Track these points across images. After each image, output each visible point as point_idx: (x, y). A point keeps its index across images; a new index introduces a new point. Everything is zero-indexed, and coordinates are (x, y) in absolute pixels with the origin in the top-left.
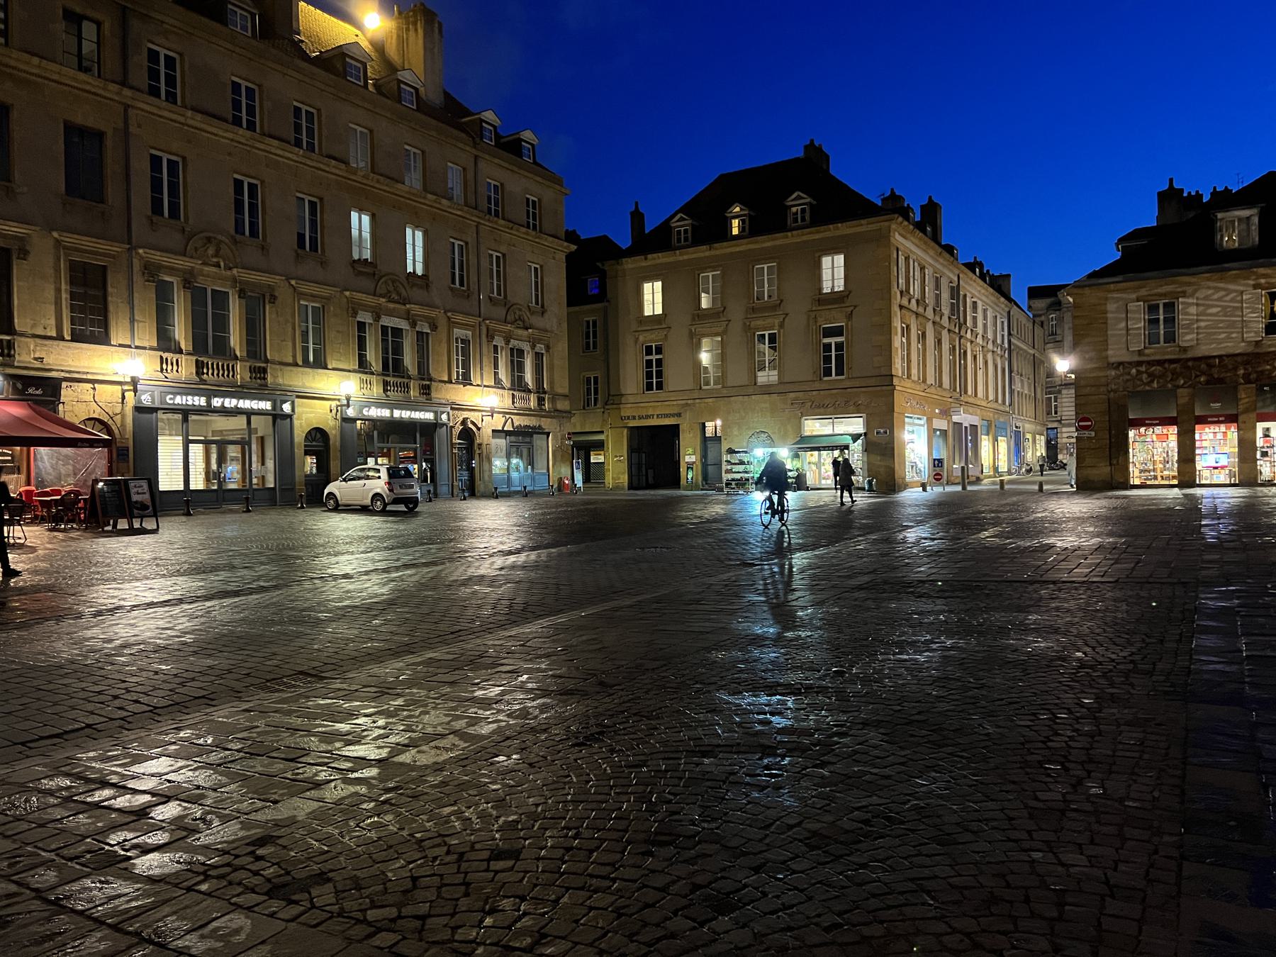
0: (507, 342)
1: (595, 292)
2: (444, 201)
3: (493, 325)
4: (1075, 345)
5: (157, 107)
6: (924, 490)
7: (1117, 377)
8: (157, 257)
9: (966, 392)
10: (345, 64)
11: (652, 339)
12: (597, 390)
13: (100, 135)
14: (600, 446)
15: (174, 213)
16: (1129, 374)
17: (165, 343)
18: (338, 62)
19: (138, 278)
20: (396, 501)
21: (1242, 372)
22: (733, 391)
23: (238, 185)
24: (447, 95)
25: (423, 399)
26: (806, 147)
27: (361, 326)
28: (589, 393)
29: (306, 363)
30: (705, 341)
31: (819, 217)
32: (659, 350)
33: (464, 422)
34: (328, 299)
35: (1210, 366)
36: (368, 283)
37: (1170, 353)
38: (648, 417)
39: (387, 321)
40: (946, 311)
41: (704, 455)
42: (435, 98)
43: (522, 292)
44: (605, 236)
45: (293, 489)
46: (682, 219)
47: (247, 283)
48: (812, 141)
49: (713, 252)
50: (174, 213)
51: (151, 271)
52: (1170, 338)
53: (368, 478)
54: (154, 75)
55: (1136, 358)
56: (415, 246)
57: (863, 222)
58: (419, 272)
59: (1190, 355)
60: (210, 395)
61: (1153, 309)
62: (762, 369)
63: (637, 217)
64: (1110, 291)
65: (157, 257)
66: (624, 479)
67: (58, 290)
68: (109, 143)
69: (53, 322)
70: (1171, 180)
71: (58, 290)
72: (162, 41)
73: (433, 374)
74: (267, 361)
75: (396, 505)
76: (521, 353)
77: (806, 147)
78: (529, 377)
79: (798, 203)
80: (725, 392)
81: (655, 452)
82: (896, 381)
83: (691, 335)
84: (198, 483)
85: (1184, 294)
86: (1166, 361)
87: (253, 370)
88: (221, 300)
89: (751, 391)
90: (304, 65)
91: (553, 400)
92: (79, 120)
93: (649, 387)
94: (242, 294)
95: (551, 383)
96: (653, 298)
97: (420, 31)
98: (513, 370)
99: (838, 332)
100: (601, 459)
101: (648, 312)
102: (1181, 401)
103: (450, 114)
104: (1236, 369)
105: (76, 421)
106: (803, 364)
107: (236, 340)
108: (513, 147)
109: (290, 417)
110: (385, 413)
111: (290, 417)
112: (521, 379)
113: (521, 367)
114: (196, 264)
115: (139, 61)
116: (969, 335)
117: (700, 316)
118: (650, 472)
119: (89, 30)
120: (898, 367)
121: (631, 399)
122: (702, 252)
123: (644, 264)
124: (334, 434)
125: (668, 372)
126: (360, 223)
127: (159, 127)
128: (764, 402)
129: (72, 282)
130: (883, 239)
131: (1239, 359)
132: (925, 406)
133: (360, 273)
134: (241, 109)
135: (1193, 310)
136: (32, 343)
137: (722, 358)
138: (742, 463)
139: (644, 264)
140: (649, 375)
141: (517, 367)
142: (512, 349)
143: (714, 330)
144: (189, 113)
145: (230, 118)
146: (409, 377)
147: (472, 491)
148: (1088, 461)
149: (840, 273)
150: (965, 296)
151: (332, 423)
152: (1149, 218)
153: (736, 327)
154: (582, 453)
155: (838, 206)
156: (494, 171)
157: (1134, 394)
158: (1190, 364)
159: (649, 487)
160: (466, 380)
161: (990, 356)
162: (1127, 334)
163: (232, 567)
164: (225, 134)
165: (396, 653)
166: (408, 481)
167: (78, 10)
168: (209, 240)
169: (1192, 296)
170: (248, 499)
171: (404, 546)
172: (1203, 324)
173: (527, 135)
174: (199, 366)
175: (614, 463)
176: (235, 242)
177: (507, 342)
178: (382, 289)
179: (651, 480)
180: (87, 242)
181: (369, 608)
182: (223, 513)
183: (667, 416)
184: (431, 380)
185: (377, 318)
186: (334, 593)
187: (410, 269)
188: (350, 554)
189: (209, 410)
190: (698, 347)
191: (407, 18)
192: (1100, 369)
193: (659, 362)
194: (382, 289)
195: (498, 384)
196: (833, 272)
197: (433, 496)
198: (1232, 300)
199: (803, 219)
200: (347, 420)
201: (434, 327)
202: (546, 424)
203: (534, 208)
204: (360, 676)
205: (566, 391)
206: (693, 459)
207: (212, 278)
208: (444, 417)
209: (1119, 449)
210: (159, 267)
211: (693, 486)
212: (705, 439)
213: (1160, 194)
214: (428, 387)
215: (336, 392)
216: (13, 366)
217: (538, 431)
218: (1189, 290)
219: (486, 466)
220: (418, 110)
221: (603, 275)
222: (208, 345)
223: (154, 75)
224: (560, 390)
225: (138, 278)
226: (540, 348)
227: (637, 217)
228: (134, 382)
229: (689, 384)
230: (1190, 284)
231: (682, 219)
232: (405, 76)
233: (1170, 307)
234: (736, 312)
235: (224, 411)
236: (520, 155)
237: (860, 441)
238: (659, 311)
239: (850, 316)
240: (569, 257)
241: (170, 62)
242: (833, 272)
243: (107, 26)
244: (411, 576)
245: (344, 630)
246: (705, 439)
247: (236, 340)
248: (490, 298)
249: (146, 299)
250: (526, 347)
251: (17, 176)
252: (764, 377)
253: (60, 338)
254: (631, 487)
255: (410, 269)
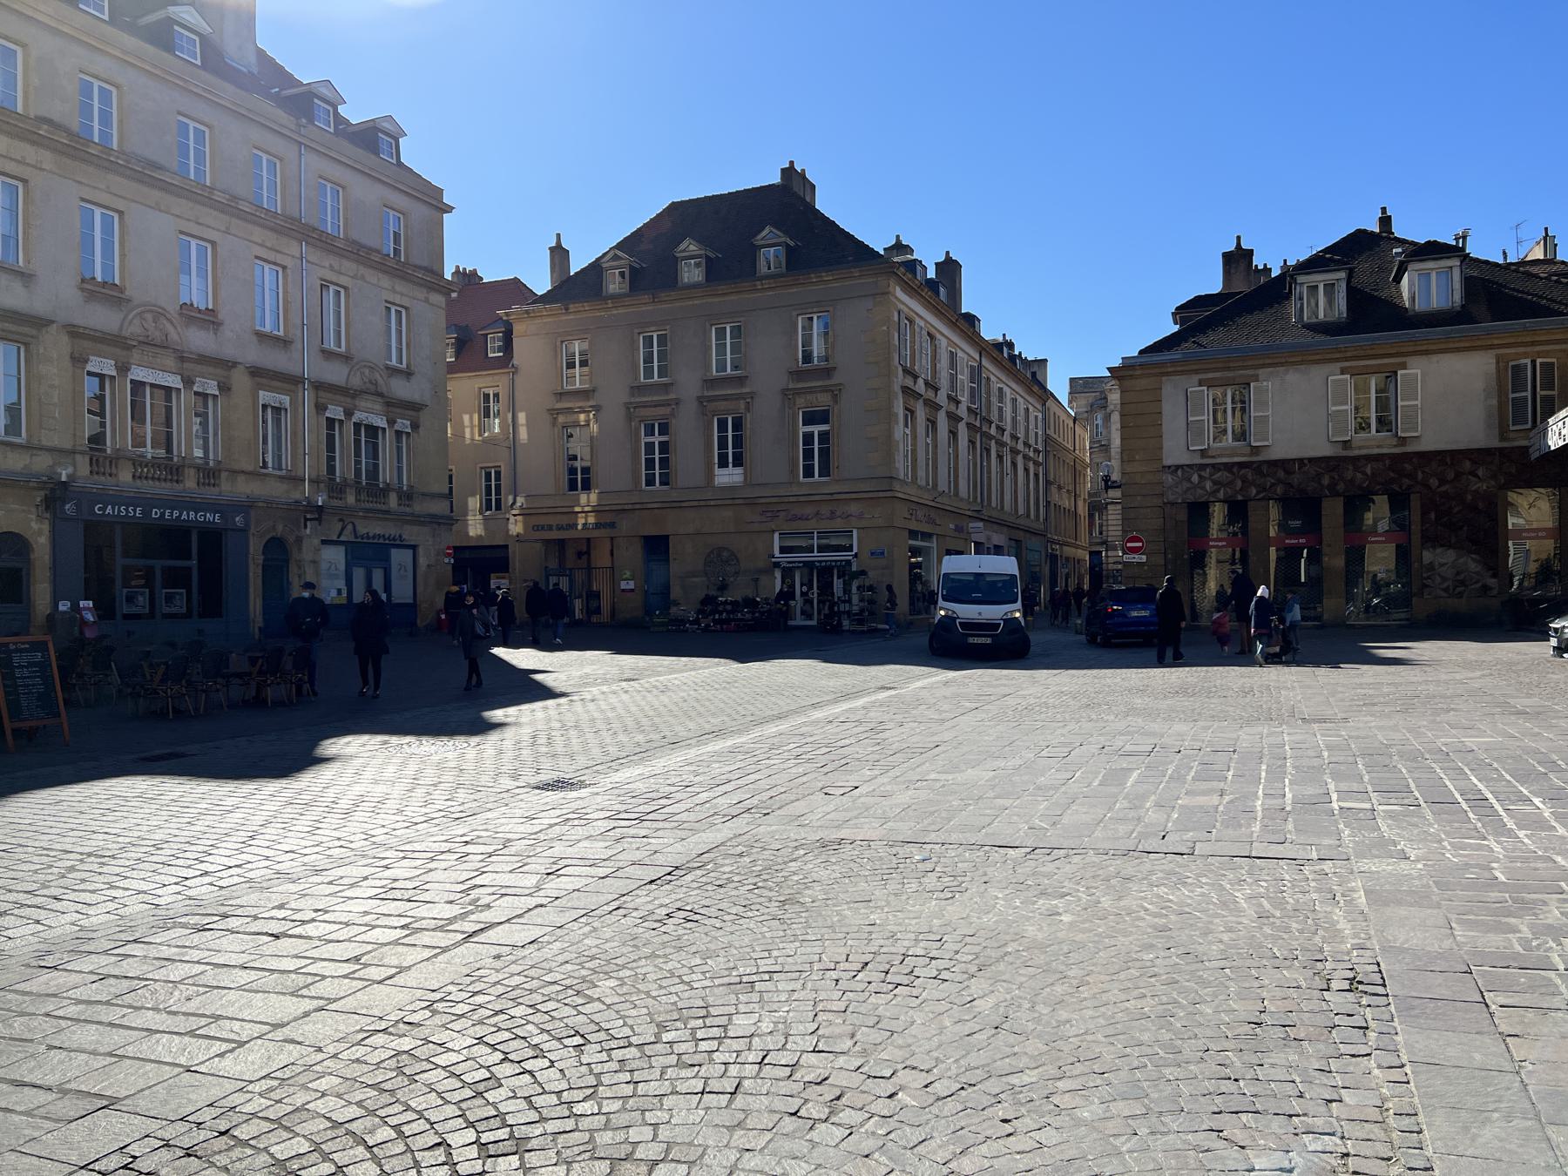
16: (1189, 480)
32: (664, 430)
48: (792, 163)
52: (1242, 435)
55: (1198, 460)
59: (1409, 449)
63: (559, 254)
70: (1239, 238)
79: (770, 255)
140: (664, 462)
142: (357, 426)
152: (1212, 282)
161: (1020, 459)
213: (1225, 255)
220: (204, 67)
227: (559, 254)
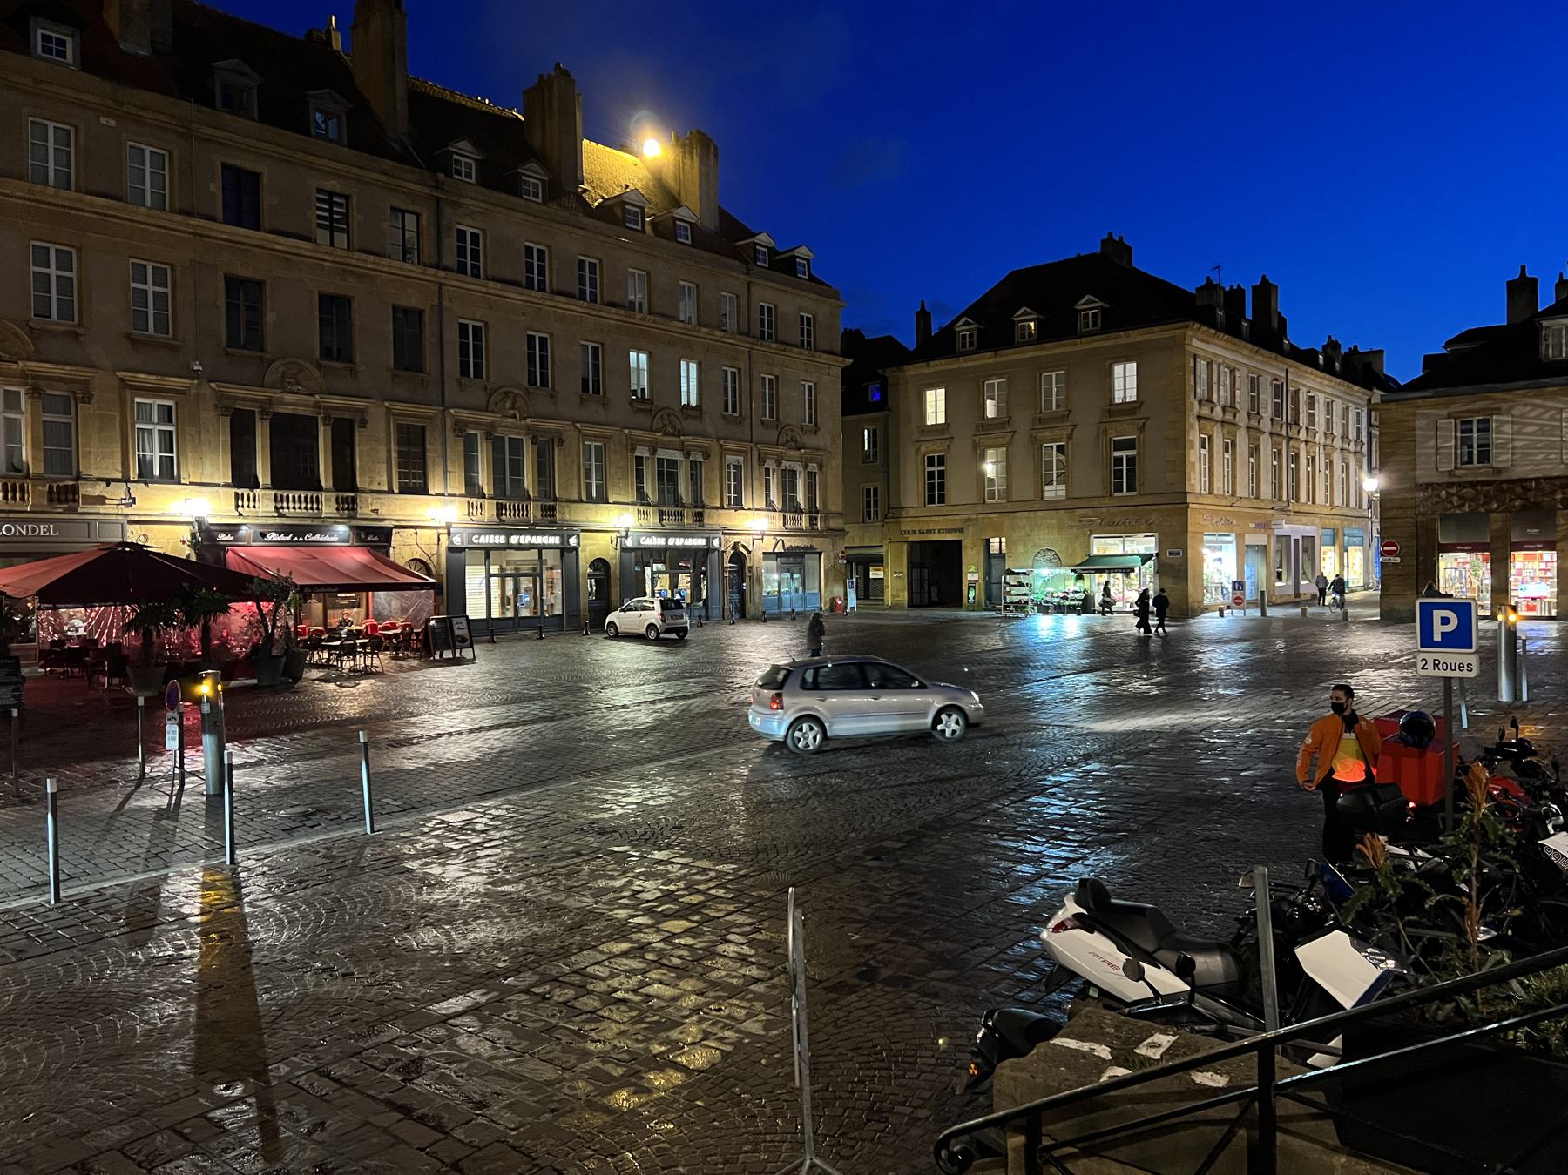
0: (779, 464)
1: (877, 398)
2: (718, 333)
3: (765, 449)
4: (1382, 466)
5: (467, 283)
6: (1221, 615)
7: (1426, 499)
8: (465, 414)
9: (1298, 500)
10: (624, 211)
11: (935, 450)
12: (874, 500)
13: (421, 313)
14: (879, 561)
15: (478, 374)
17: (472, 489)
18: (617, 211)
19: (450, 434)
20: (668, 631)
21: (1559, 496)
22: (1019, 505)
23: (531, 339)
24: (722, 212)
25: (696, 526)
26: (1103, 242)
27: (639, 460)
28: (869, 506)
29: (590, 500)
30: (990, 452)
31: (1111, 322)
32: (941, 461)
33: (735, 546)
34: (609, 438)
35: (1526, 490)
36: (643, 420)
37: (1486, 474)
38: (929, 532)
39: (663, 454)
40: (1267, 414)
41: (988, 572)
42: (711, 223)
43: (795, 411)
44: (890, 337)
45: (578, 616)
46: (966, 323)
47: (537, 430)
48: (1110, 235)
49: (998, 359)
50: (478, 374)
51: (460, 427)
52: (1485, 456)
53: (644, 609)
54: (461, 252)
55: (1446, 479)
56: (689, 375)
57: (1156, 329)
58: (693, 404)
59: (1504, 477)
60: (508, 533)
61: (1466, 427)
62: (1050, 483)
63: (923, 317)
64: (1419, 407)
65: (465, 414)
66: (904, 596)
67: (389, 451)
68: (427, 318)
69: (385, 478)
70: (1523, 268)
71: (389, 451)
72: (471, 222)
73: (706, 502)
74: (555, 500)
75: (669, 636)
76: (793, 473)
77: (1103, 242)
78: (801, 497)
79: (1089, 305)
80: (1010, 507)
81: (936, 570)
82: (1190, 499)
83: (975, 446)
84: (496, 614)
85: (1499, 411)
86: (1478, 483)
87: (543, 508)
88: (516, 445)
89: (1037, 506)
90: (584, 220)
91: (825, 519)
92: (404, 303)
93: (931, 500)
94: (534, 441)
95: (824, 502)
96: (935, 406)
97: (696, 158)
98: (784, 491)
99: (1129, 445)
100: (880, 575)
101: (930, 421)
102: (1496, 526)
103: (724, 239)
104: (1553, 492)
105: (401, 563)
106: (1091, 480)
107: (529, 482)
108: (784, 265)
109: (576, 549)
110: (660, 542)
111: (576, 549)
112: (793, 499)
113: (793, 488)
114: (497, 418)
115: (451, 243)
116: (1303, 435)
117: (984, 425)
118: (934, 590)
119: (410, 220)
120: (1195, 481)
121: (912, 512)
122: (987, 359)
123: (926, 371)
124: (614, 562)
125: (950, 483)
126: (638, 360)
127: (468, 299)
128: (1052, 518)
129: (399, 443)
130: (1178, 346)
131: (1557, 482)
132: (1227, 522)
133: (639, 410)
134: (533, 273)
135: (1508, 428)
136: (369, 497)
137: (1008, 469)
138: (1021, 585)
139: (926, 371)
140: (931, 488)
141: (788, 489)
143: (1000, 441)
144: (491, 284)
145: (524, 281)
146: (683, 506)
147: (742, 613)
148: (1393, 589)
149: (1132, 382)
150: (1297, 392)
151: (612, 553)
153: (1022, 439)
154: (861, 568)
155: (1137, 303)
156: (767, 293)
157: (1446, 518)
158: (1505, 486)
159: (932, 604)
160: (737, 505)
161: (1336, 458)
162: (1437, 453)
163: (543, 698)
164: (517, 296)
165: (651, 761)
166: (678, 612)
167: (402, 207)
168: (506, 393)
169: (1507, 413)
170: (540, 626)
171: (669, 679)
172: (1518, 444)
173: (803, 251)
174: (499, 507)
175: (893, 579)
176: (529, 394)
177: (779, 464)
178: (658, 424)
179: (935, 598)
180: (411, 408)
181: (638, 732)
182: (520, 639)
183: (949, 531)
184: (703, 507)
185: (653, 452)
186: (616, 719)
187: (684, 402)
188: (627, 681)
189: (507, 547)
190: (983, 458)
191: (684, 146)
192: (1407, 490)
193: (941, 474)
194: (658, 424)
195: (770, 506)
196: (1125, 381)
197: (704, 619)
198: (1552, 418)
199: (1095, 324)
200: (624, 550)
201: (707, 456)
202: (817, 543)
203: (809, 324)
204: (631, 770)
205: (840, 509)
206: (975, 577)
207: (509, 428)
208: (716, 542)
209: (1428, 573)
210: (466, 423)
211: (974, 606)
212: (989, 556)
213: (1509, 283)
214: (701, 514)
215: (615, 524)
216: (355, 518)
217: (810, 550)
218: (1504, 406)
219: (756, 588)
221: (884, 382)
222: (507, 489)
223: (461, 252)
224: (833, 508)
225: (450, 434)
226: (813, 467)
227: (923, 317)
228: (448, 527)
229: (971, 497)
230: (1505, 401)
231: (966, 323)
232: (681, 213)
233: (1485, 427)
234: (1022, 421)
235: (519, 547)
236: (794, 273)
237: (1151, 562)
238: (941, 420)
239: (1142, 429)
240: (845, 372)
241: (475, 237)
242: (1125, 381)
243: (425, 216)
244: (670, 708)
245: (621, 746)
246: (989, 556)
247: (529, 482)
248: (762, 422)
249: (456, 450)
250: (798, 467)
251: (358, 357)
252: (1054, 491)
253: (391, 492)
254: (912, 605)
255: (684, 402)
